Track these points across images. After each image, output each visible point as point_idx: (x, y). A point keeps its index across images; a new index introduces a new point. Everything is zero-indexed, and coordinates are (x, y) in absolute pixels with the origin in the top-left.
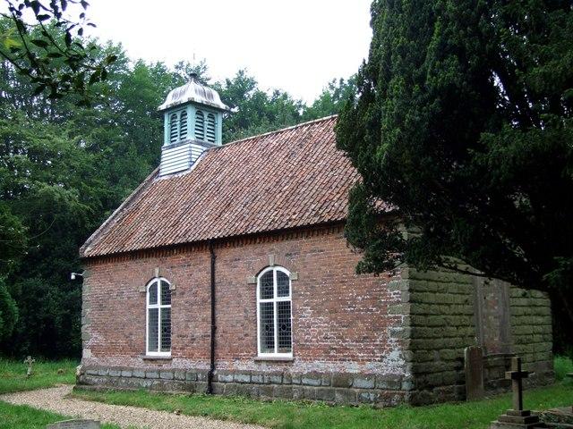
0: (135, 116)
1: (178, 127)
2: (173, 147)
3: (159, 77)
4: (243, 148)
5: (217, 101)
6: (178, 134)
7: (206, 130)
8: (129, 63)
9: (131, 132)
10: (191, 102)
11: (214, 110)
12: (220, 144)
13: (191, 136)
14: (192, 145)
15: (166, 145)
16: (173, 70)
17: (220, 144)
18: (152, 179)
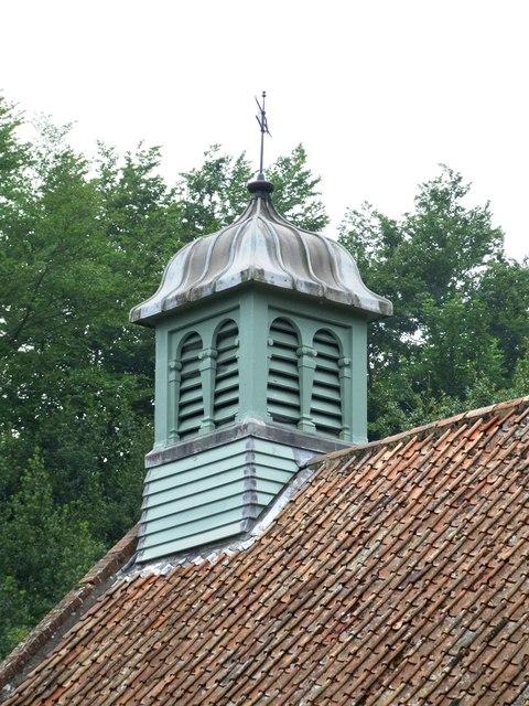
0: (44, 364)
1: (206, 379)
2: (186, 453)
3: (133, 221)
4: (448, 444)
5: (349, 284)
6: (206, 406)
7: (308, 390)
8: (28, 172)
9: (31, 425)
10: (253, 287)
11: (335, 313)
12: (362, 442)
13: (252, 414)
14: (259, 446)
15: (160, 446)
16: (185, 196)
17: (362, 442)
18: (108, 573)
